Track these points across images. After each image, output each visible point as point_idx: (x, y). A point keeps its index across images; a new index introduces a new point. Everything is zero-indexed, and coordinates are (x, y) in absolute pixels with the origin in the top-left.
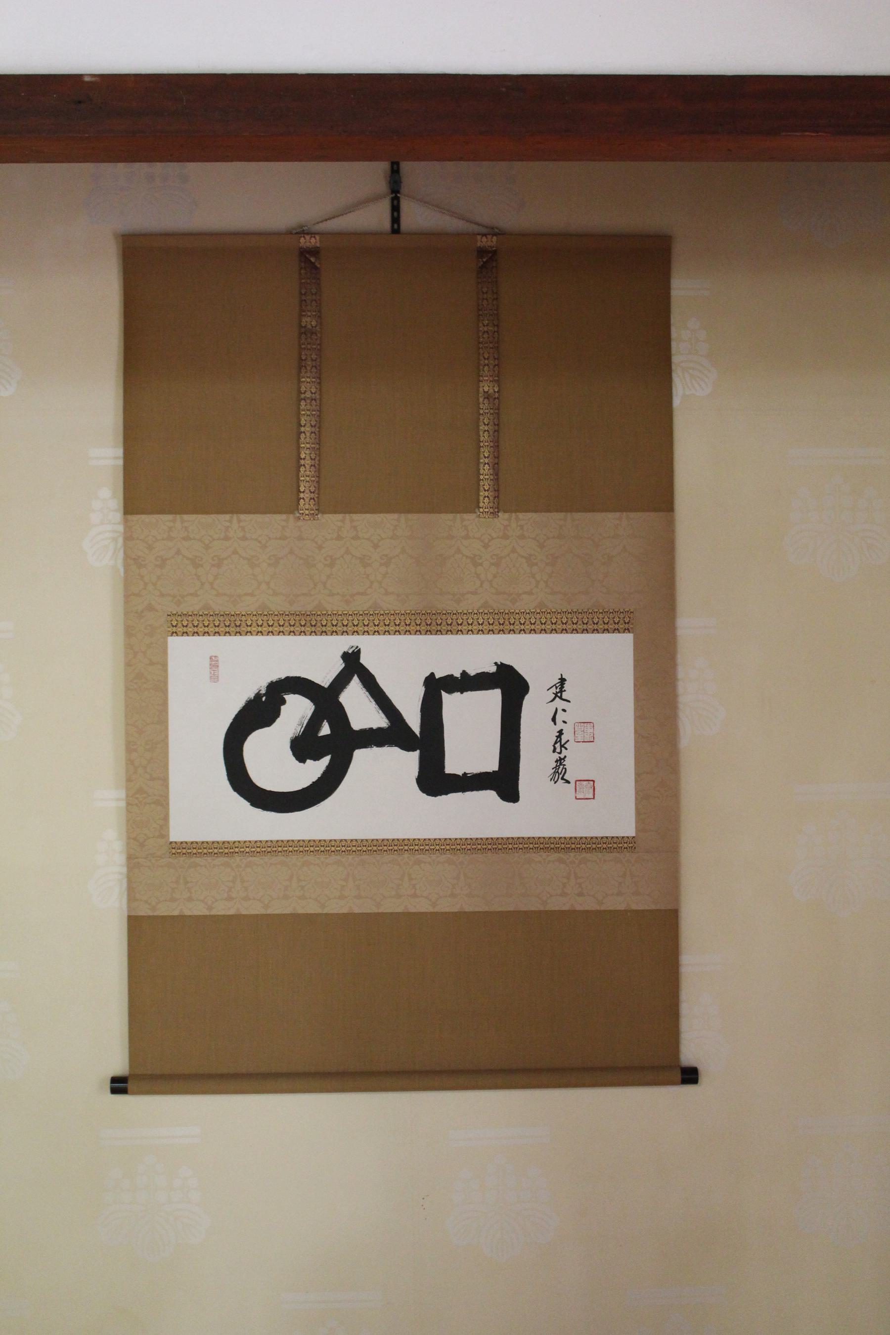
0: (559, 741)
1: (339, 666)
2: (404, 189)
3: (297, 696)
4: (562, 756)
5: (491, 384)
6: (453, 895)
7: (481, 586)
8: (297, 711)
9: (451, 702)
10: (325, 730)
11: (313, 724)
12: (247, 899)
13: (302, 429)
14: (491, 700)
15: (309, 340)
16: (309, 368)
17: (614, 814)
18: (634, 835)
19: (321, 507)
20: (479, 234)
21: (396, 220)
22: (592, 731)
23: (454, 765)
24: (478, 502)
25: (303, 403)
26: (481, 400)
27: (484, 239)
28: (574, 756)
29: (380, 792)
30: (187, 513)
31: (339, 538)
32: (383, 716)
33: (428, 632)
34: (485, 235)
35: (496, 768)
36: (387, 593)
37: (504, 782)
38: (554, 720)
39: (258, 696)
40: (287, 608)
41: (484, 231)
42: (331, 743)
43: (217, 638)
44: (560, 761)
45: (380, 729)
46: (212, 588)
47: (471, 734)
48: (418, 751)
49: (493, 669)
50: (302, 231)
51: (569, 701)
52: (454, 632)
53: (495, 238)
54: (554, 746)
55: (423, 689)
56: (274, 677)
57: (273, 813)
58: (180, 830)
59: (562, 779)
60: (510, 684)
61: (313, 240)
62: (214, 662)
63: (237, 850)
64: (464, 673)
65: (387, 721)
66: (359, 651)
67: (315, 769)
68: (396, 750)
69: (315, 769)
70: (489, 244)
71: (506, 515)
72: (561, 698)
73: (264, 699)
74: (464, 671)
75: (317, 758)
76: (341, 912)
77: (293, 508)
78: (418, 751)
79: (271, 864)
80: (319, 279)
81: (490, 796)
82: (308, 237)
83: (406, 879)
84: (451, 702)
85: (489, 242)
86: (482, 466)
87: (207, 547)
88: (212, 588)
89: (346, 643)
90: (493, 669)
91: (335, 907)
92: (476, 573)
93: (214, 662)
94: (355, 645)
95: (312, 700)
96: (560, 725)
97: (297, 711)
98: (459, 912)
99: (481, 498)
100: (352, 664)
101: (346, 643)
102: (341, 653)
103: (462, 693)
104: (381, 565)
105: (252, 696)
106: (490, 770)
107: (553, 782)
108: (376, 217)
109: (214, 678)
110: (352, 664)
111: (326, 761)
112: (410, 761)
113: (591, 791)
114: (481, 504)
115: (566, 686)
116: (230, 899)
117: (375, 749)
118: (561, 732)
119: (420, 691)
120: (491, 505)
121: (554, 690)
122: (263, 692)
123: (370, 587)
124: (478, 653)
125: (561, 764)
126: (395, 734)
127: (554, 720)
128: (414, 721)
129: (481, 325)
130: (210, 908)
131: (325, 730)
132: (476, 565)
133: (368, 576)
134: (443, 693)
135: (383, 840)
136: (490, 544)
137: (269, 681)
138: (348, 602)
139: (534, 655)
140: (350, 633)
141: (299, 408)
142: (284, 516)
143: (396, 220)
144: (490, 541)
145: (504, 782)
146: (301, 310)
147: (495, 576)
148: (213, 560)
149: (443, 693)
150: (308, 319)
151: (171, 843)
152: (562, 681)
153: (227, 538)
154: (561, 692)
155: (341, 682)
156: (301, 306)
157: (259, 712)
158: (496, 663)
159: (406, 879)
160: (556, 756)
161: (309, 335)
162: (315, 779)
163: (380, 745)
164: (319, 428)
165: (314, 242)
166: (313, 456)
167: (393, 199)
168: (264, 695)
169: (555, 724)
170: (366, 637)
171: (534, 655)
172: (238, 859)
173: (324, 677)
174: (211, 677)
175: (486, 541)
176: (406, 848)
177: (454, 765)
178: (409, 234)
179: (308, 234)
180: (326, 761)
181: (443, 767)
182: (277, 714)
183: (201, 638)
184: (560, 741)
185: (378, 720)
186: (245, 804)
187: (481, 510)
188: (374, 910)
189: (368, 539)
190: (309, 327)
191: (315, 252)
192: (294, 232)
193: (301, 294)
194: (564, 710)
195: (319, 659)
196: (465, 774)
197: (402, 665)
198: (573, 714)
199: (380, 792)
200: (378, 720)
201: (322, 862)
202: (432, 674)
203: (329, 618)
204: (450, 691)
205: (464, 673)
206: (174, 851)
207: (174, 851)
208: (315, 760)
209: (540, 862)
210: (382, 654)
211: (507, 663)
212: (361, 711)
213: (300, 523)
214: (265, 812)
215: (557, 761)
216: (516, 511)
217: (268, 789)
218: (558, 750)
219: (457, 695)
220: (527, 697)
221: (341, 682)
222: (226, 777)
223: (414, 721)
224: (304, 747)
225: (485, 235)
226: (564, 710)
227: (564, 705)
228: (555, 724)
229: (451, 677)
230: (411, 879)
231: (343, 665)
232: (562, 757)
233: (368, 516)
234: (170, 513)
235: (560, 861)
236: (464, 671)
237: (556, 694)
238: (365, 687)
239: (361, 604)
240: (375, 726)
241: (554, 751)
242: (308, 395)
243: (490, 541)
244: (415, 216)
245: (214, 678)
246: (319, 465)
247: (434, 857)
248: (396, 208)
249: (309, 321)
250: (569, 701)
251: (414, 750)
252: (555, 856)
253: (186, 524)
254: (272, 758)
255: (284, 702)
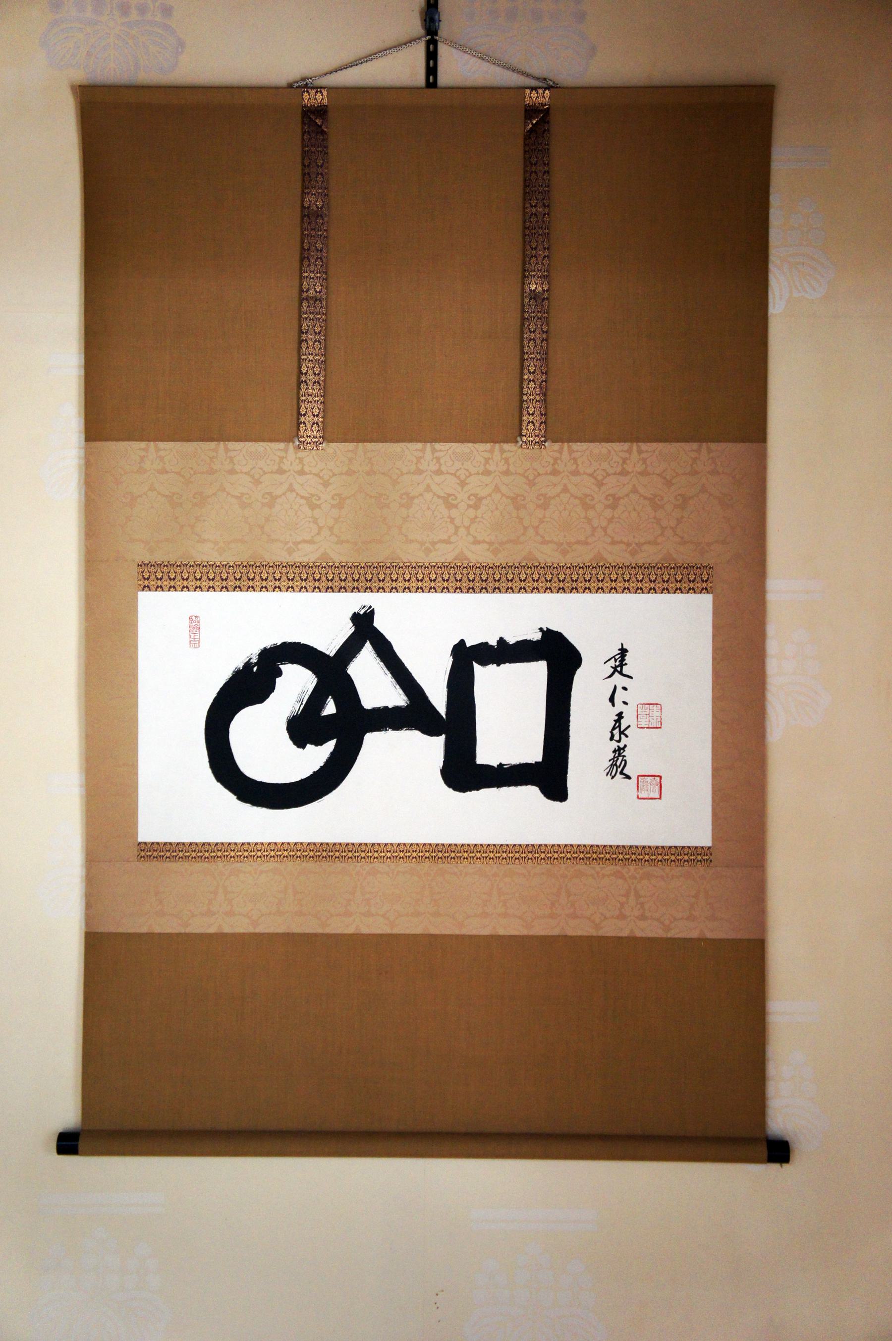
0: (618, 727)
1: (348, 629)
2: (444, 30)
3: (295, 665)
4: (621, 745)
5: (539, 281)
6: (552, 916)
7: (456, 533)
8: (295, 684)
9: (485, 676)
10: (330, 708)
11: (316, 700)
12: (368, 914)
13: (304, 337)
14: (535, 674)
15: (313, 225)
16: (312, 260)
17: (685, 819)
18: (710, 844)
19: (551, 432)
20: (527, 88)
21: (432, 71)
22: (659, 714)
23: (488, 753)
24: (521, 430)
25: (305, 304)
26: (526, 300)
27: (534, 94)
28: (634, 742)
29: (396, 788)
30: (162, 440)
31: (555, 473)
32: (401, 692)
33: (471, 590)
34: (533, 89)
35: (539, 758)
36: (476, 542)
37: (549, 775)
38: (612, 700)
39: (248, 665)
40: (628, 559)
41: (534, 83)
42: (337, 725)
43: (198, 593)
44: (619, 751)
45: (396, 708)
46: (332, 534)
47: (509, 714)
48: (444, 736)
49: (538, 636)
50: (305, 85)
51: (631, 677)
52: (244, 589)
53: (547, 92)
54: (611, 732)
55: (451, 659)
56: (269, 643)
57: (264, 809)
58: (152, 828)
59: (622, 773)
60: (557, 654)
61: (319, 96)
62: (194, 624)
63: (219, 854)
64: (501, 641)
65: (406, 698)
66: (373, 611)
67: (317, 756)
68: (416, 734)
69: (317, 756)
70: (540, 100)
71: (556, 446)
72: (621, 673)
73: (255, 669)
74: (501, 638)
75: (319, 742)
76: (346, 932)
77: (293, 434)
78: (444, 736)
79: (261, 872)
80: (326, 147)
81: (532, 792)
82: (312, 92)
83: (632, 897)
84: (485, 676)
85: (543, 97)
86: (525, 383)
87: (463, 484)
88: (606, 534)
89: (356, 602)
90: (538, 636)
91: (477, 927)
92: (449, 517)
93: (194, 624)
94: (368, 604)
95: (314, 672)
96: (619, 707)
97: (295, 684)
98: (492, 936)
99: (524, 424)
100: (364, 628)
101: (356, 602)
102: (351, 614)
103: (498, 665)
104: (676, 506)
105: (241, 666)
106: (531, 760)
107: (609, 777)
108: (405, 68)
109: (195, 642)
110: (364, 628)
111: (331, 745)
112: (431, 749)
113: (657, 788)
114: (524, 432)
115: (628, 659)
116: (622, 917)
117: (390, 732)
118: (620, 715)
119: (447, 662)
120: (537, 432)
121: (612, 663)
122: (254, 660)
123: (456, 533)
124: (517, 616)
125: (620, 755)
126: (415, 714)
127: (612, 700)
128: (439, 699)
129: (528, 205)
130: (668, 929)
131: (330, 708)
132: (313, 507)
133: (177, 518)
134: (476, 665)
135: (347, 844)
136: (589, 481)
137: (262, 647)
138: (564, 553)
139: (586, 619)
140: (192, 589)
141: (300, 311)
142: (282, 445)
143: (432, 71)
144: (535, 477)
145: (549, 775)
146: (304, 187)
147: (541, 521)
148: (401, 498)
149: (476, 665)
150: (313, 198)
151: (140, 843)
152: (623, 652)
153: (281, 471)
154: (622, 665)
155: (350, 649)
156: (303, 181)
157: (250, 684)
158: (541, 629)
159: (632, 897)
160: (614, 745)
161: (313, 219)
162: (316, 768)
163: (397, 727)
164: (325, 335)
165: (321, 98)
166: (317, 371)
167: (428, 43)
168: (256, 664)
169: (613, 705)
170: (381, 595)
171: (586, 619)
172: (221, 865)
173: (329, 642)
174: (192, 641)
175: (531, 477)
176: (350, 854)
177: (488, 753)
178: (445, 88)
179: (312, 88)
180: (331, 745)
181: (474, 756)
182: (271, 688)
183: (205, 593)
184: (620, 726)
185: (396, 698)
186: (232, 797)
187: (524, 439)
188: (387, 930)
189: (591, 475)
190: (314, 208)
191: (321, 111)
192: (296, 85)
193: (303, 165)
194: (625, 689)
195: (322, 620)
196: (501, 765)
197: (426, 629)
198: (635, 694)
199: (396, 788)
200: (396, 698)
201: (598, 873)
202: (462, 642)
203: (401, 571)
204: (483, 663)
205: (501, 641)
206: (143, 854)
207: (143, 854)
208: (316, 745)
209: (662, 877)
210: (394, 613)
211: (555, 629)
212: (374, 686)
213: (301, 454)
214: (255, 808)
215: (615, 751)
216: (570, 440)
217: (259, 779)
218: (617, 737)
219: (492, 667)
220: (579, 672)
221: (350, 649)
222: (208, 764)
223: (439, 699)
224: (303, 729)
225: (533, 89)
226: (625, 689)
227: (625, 682)
228: (613, 705)
229: (485, 645)
230: (569, 894)
231: (353, 629)
232: (622, 745)
233: (455, 445)
234: (141, 439)
235: (618, 875)
236: (501, 638)
237: (615, 669)
238: (378, 656)
239: (443, 555)
240: (390, 705)
241: (612, 738)
242: (312, 293)
243: (604, 478)
244: (455, 68)
245: (195, 642)
246: (325, 381)
247: (461, 867)
248: (432, 56)
249: (314, 201)
250: (631, 677)
251: (438, 735)
252: (610, 869)
253: (162, 453)
254: (264, 741)
255: (279, 673)
